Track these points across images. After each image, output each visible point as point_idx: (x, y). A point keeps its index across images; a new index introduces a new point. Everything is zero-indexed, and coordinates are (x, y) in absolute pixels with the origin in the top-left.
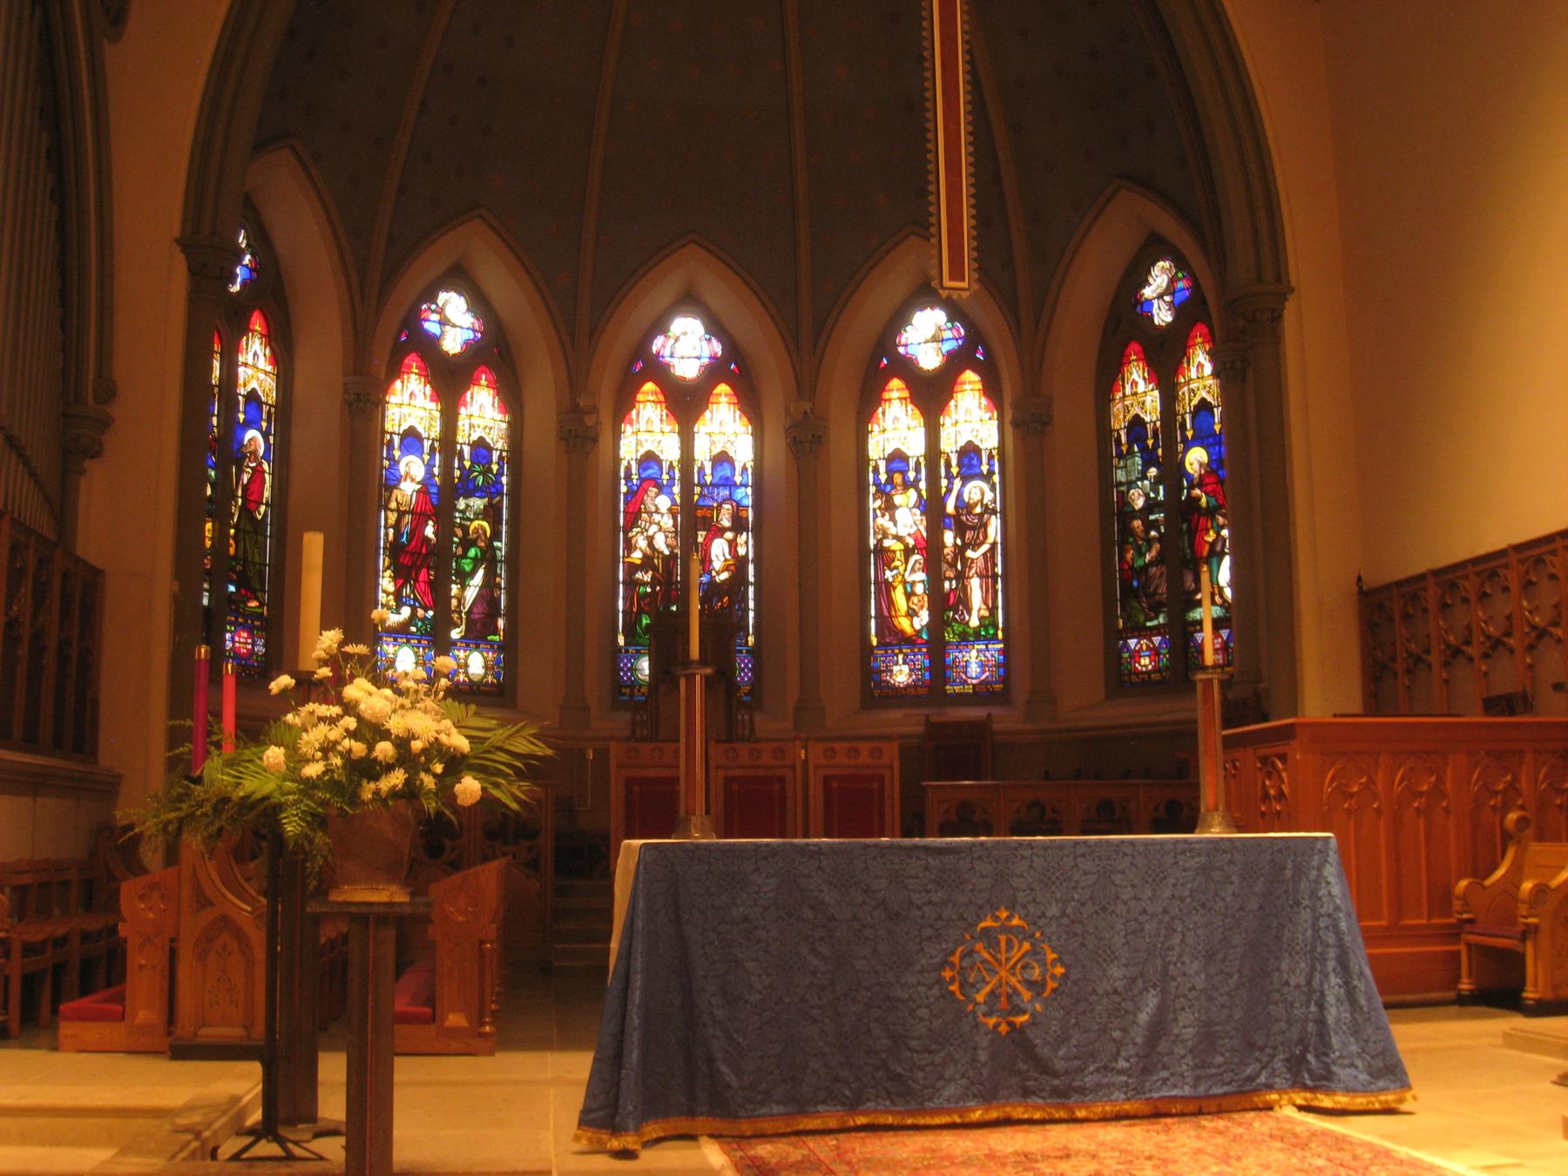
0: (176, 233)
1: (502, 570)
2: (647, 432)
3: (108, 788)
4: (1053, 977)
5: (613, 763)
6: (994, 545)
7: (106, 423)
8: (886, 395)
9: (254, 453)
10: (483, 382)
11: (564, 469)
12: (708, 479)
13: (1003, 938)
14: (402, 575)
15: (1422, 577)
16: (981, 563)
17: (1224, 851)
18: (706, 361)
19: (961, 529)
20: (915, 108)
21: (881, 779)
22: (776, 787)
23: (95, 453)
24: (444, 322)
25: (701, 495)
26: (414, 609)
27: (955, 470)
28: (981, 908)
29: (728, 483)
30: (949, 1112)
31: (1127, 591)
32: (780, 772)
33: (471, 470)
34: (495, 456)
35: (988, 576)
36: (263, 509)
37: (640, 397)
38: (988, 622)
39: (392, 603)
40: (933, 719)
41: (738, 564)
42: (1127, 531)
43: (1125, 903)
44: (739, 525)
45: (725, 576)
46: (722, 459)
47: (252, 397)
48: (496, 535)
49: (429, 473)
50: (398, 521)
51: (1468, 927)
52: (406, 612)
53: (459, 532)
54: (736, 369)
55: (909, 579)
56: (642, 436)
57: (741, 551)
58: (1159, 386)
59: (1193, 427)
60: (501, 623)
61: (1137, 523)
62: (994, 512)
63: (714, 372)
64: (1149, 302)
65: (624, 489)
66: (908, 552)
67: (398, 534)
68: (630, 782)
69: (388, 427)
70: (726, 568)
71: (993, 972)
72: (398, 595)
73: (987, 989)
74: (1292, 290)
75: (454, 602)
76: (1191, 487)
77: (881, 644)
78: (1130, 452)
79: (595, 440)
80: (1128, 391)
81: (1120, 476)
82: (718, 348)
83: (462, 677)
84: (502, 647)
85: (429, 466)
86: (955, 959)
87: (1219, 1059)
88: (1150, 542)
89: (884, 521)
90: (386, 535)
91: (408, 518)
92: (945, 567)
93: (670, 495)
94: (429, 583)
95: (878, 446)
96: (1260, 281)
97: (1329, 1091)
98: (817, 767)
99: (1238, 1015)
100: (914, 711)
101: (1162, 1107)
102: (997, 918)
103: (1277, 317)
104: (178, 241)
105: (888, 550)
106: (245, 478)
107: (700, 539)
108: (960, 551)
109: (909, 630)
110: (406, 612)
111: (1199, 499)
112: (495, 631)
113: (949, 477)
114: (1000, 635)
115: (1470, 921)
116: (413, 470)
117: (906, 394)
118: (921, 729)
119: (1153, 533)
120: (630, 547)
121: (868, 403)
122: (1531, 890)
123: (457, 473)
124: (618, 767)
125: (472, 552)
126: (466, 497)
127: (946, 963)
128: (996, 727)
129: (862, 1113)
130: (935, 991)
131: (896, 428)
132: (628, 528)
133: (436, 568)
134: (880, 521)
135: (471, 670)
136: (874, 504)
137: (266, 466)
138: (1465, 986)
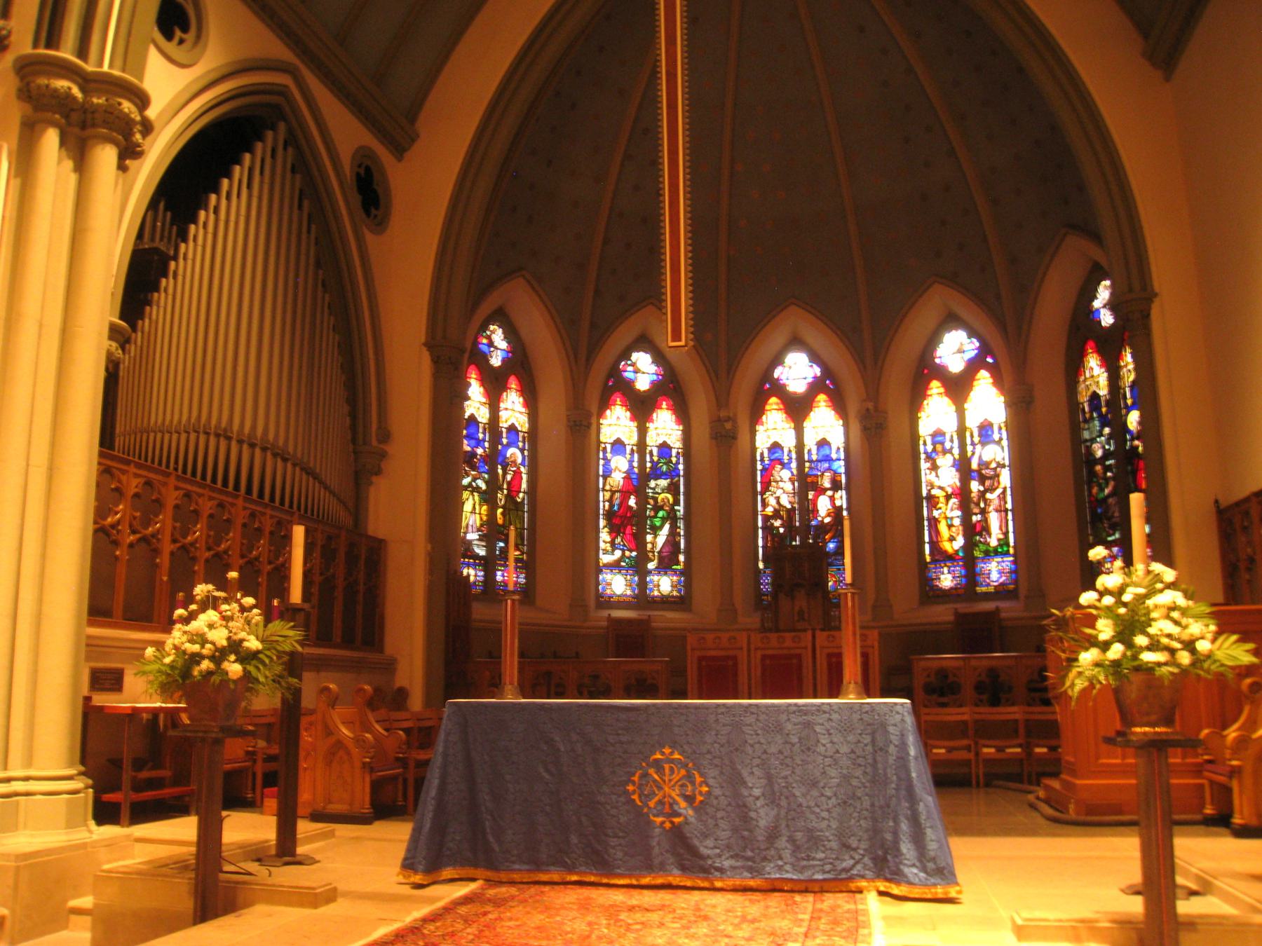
0: (423, 340)
1: (681, 524)
2: (774, 428)
3: (390, 667)
4: (701, 793)
5: (689, 648)
6: (1005, 489)
7: (383, 455)
8: (929, 392)
9: (514, 462)
10: (664, 405)
11: (721, 456)
12: (814, 457)
13: (667, 766)
14: (615, 530)
15: (1247, 500)
16: (996, 502)
17: (825, 712)
18: (810, 380)
19: (982, 479)
20: (651, 222)
21: (799, 656)
22: (731, 663)
23: (378, 472)
24: (636, 371)
25: (810, 468)
26: (623, 551)
27: (976, 439)
28: (653, 746)
29: (828, 459)
30: (630, 876)
31: (1094, 514)
32: (798, 651)
33: (658, 463)
34: (674, 452)
35: (1002, 510)
36: (521, 495)
37: (768, 407)
38: (1004, 542)
39: (609, 548)
40: (961, 611)
41: (837, 511)
42: (1092, 473)
43: (752, 746)
44: (836, 486)
45: (827, 520)
46: (823, 443)
47: (512, 429)
48: (677, 502)
49: (631, 467)
50: (612, 497)
51: (1209, 766)
52: (618, 553)
53: (651, 501)
54: (828, 385)
55: (949, 515)
56: (769, 432)
57: (838, 503)
58: (1108, 370)
59: (1132, 397)
60: (682, 558)
61: (1098, 468)
62: (1003, 466)
63: (816, 387)
64: (1098, 310)
65: (759, 467)
66: (948, 497)
67: (612, 506)
68: (701, 659)
69: (602, 439)
70: (828, 515)
71: (660, 788)
72: (612, 543)
73: (657, 799)
74: (1156, 295)
75: (649, 546)
76: (1132, 439)
77: (934, 561)
78: (1092, 418)
79: (734, 438)
80: (1088, 375)
81: (1086, 435)
82: (817, 371)
83: (656, 593)
84: (682, 573)
85: (631, 462)
86: (636, 778)
87: (821, 855)
88: (1107, 480)
89: (932, 477)
90: (603, 506)
91: (617, 495)
92: (972, 506)
93: (790, 469)
94: (633, 534)
95: (926, 426)
96: (1131, 290)
97: (898, 883)
98: (822, 647)
99: (834, 824)
100: (947, 606)
101: (778, 885)
102: (663, 754)
103: (1146, 316)
104: (425, 344)
105: (934, 497)
106: (509, 477)
107: (810, 497)
108: (982, 494)
109: (950, 551)
110: (618, 553)
111: (1137, 447)
112: (678, 563)
113: (973, 444)
114: (1012, 551)
115: (1210, 762)
116: (620, 466)
117: (942, 390)
118: (951, 618)
119: (1109, 474)
120: (765, 505)
121: (917, 396)
122: (1235, 738)
123: (649, 465)
124: (693, 650)
125: (661, 514)
126: (656, 479)
127: (630, 781)
128: (1003, 615)
129: (577, 873)
130: (622, 799)
131: (936, 413)
132: (763, 493)
133: (637, 525)
134: (929, 477)
135: (662, 588)
136: (924, 465)
137: (522, 469)
138: (1209, 810)
